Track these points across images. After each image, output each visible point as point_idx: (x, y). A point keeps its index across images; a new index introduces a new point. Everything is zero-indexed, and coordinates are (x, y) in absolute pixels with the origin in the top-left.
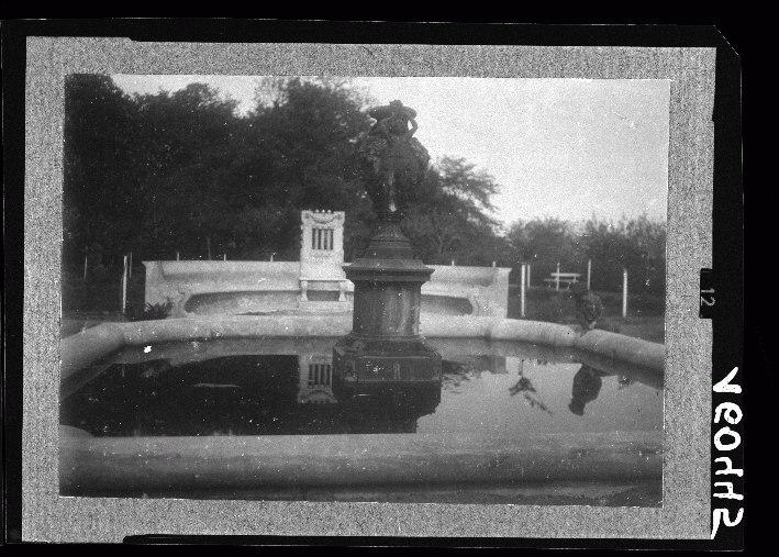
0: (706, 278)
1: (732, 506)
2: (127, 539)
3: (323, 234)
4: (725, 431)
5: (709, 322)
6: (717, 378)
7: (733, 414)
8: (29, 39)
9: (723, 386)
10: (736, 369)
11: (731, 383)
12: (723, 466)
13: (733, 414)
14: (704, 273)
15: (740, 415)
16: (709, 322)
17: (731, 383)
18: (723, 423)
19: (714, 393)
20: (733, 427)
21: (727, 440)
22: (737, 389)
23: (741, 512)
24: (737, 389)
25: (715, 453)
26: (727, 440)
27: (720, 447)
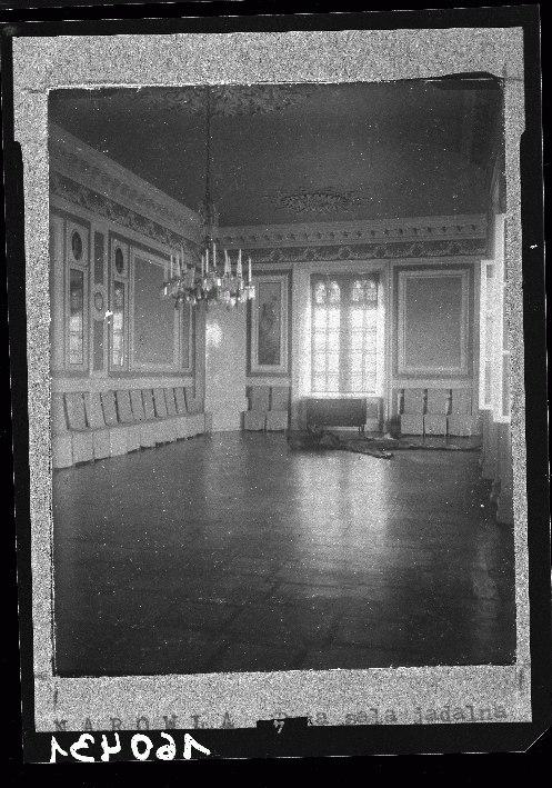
0: (297, 725)
1: (95, 750)
2: (17, 146)
3: (112, 418)
4: (150, 745)
5: (254, 726)
6: (199, 734)
7: (166, 753)
8: (519, 31)
9: (189, 742)
10: (208, 752)
11: (193, 748)
12: (112, 743)
13: (166, 753)
14: (304, 720)
15: (165, 758)
16: (254, 726)
17: (193, 748)
18: (159, 742)
19: (114, 732)
20: (153, 751)
21: (142, 747)
22: (187, 755)
23: (91, 760)
24: (187, 755)
25: (126, 737)
26: (142, 747)
27: (137, 739)
